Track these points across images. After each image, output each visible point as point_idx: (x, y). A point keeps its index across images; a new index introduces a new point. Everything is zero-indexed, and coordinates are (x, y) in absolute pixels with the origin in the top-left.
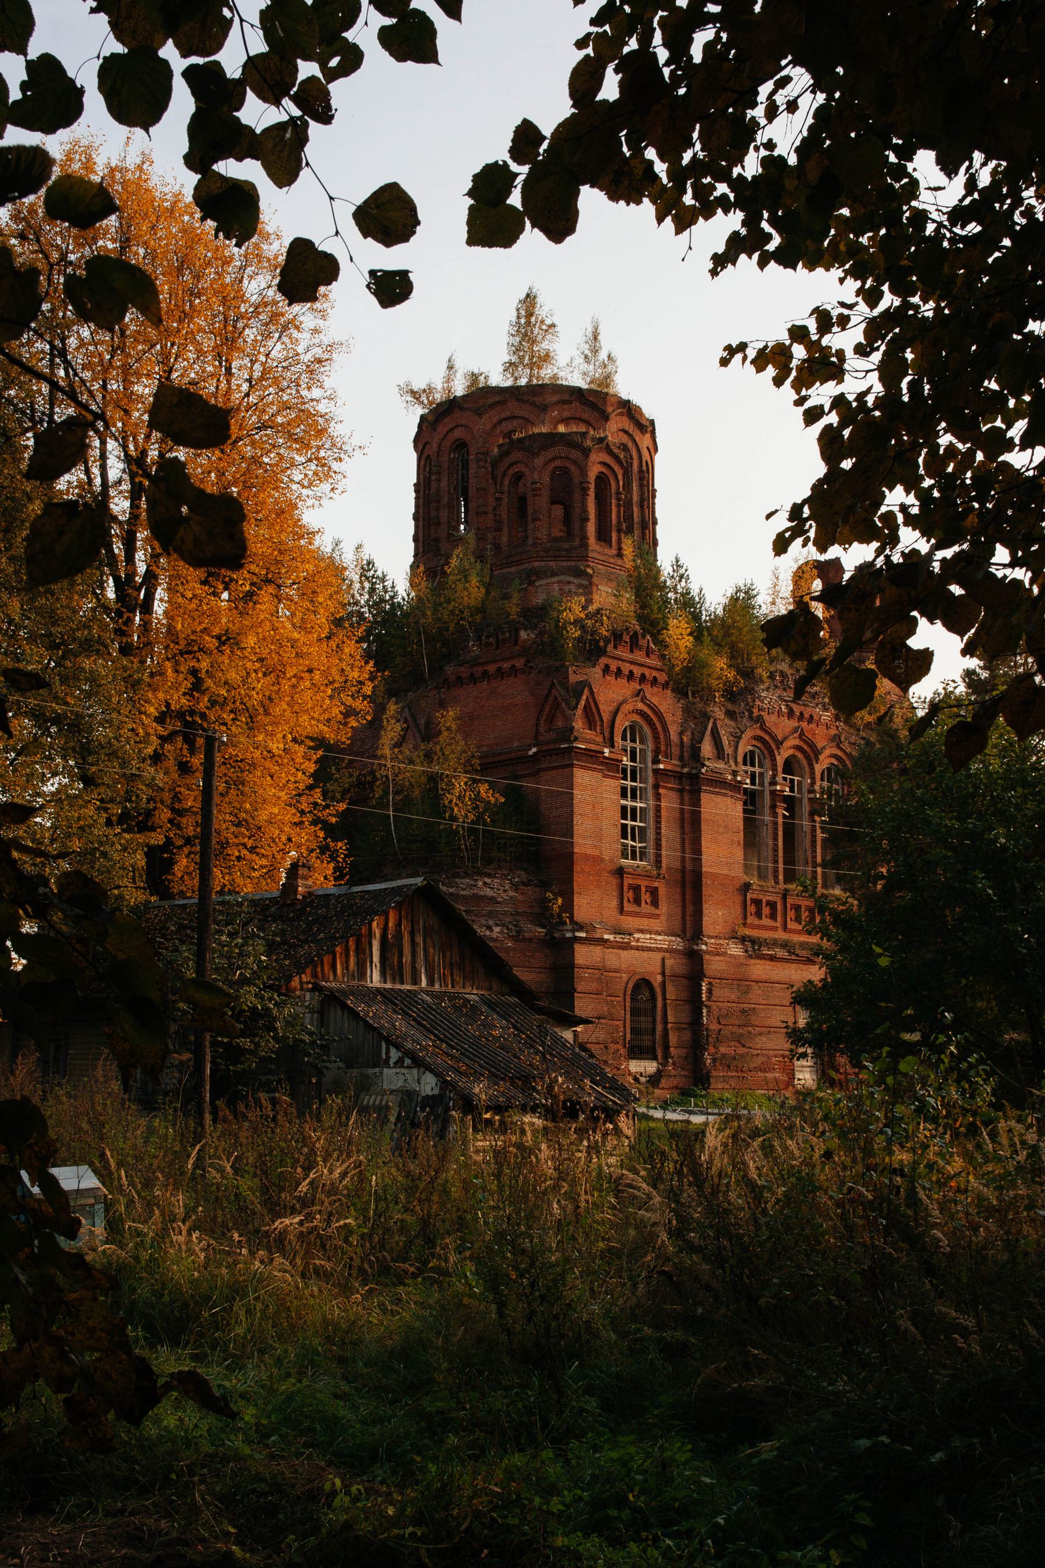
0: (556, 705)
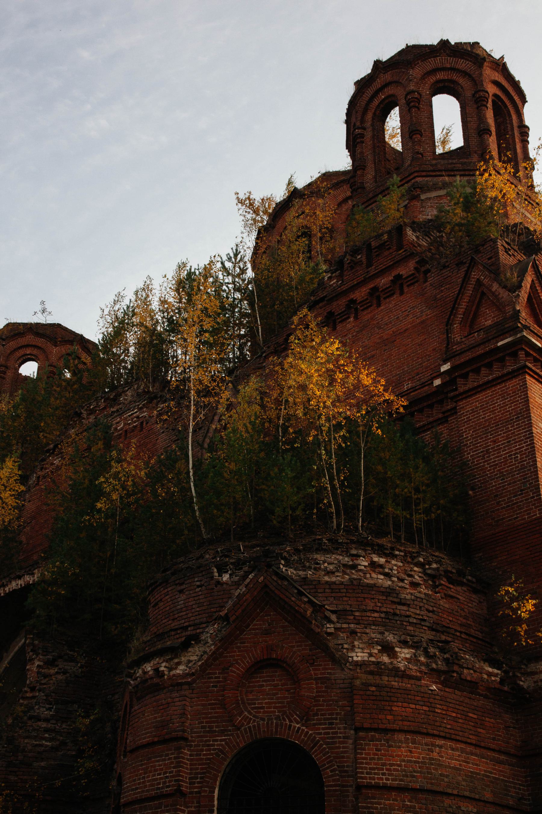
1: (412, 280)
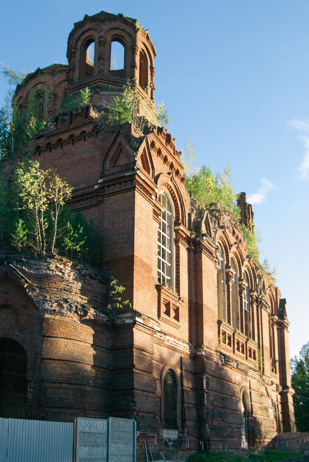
0: (121, 149)
1: (91, 135)
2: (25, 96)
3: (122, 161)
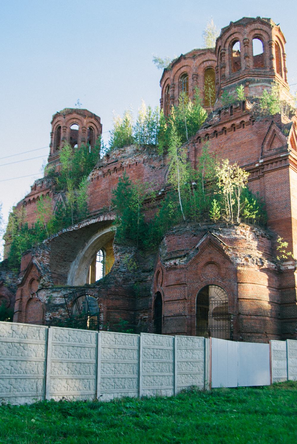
0: (274, 135)
1: (248, 123)
2: (172, 77)
3: (277, 145)
